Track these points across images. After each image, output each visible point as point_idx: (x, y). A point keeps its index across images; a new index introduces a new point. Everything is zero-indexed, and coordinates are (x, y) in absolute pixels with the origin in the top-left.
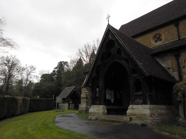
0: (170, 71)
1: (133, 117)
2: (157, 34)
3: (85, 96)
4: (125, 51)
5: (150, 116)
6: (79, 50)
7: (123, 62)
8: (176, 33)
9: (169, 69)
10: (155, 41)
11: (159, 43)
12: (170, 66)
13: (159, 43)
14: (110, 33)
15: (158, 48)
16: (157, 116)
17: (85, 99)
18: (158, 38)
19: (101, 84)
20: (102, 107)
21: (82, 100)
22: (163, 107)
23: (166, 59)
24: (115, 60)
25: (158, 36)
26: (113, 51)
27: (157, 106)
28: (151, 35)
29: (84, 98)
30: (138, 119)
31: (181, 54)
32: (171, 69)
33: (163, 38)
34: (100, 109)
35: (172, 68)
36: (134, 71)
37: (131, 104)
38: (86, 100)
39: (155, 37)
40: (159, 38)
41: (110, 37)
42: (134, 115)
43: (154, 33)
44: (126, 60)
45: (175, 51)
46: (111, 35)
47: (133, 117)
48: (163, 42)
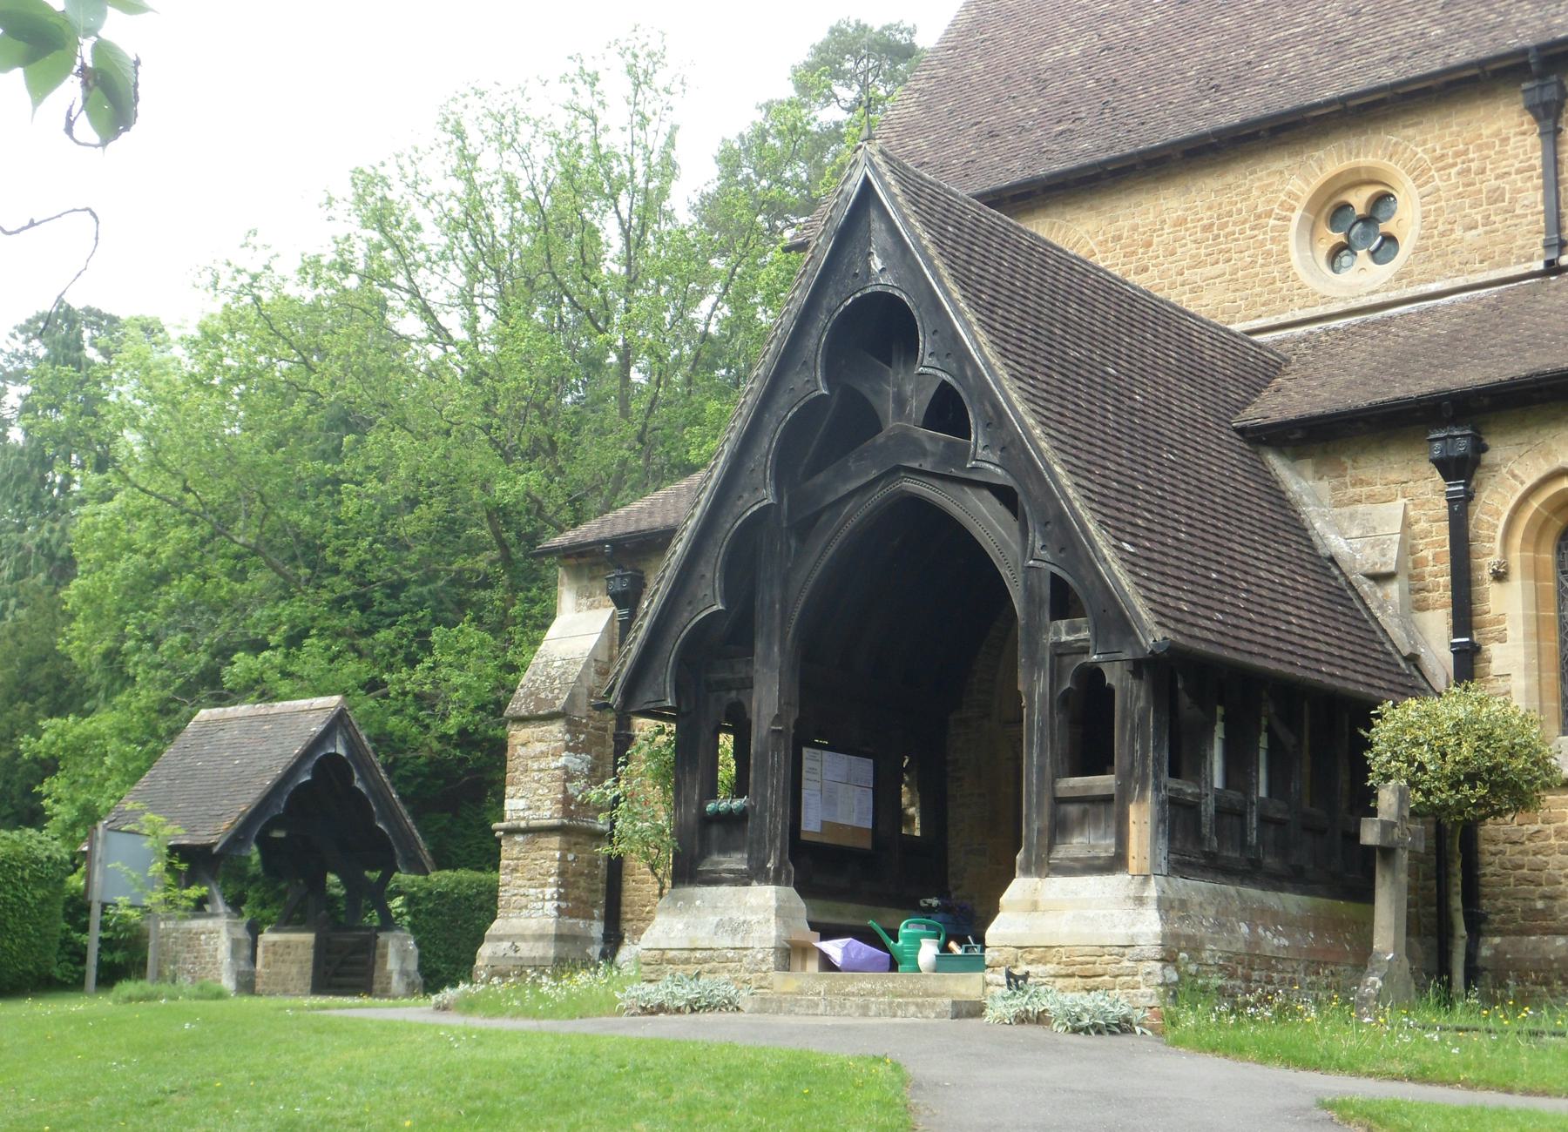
0: (1387, 602)
1: (1031, 969)
2: (1356, 170)
3: (548, 814)
4: (997, 420)
5: (1161, 960)
6: (365, 182)
7: (984, 518)
8: (1533, 197)
9: (1380, 578)
10: (1324, 248)
11: (1364, 279)
12: (1393, 552)
13: (1364, 279)
14: (877, 225)
15: (1347, 333)
16: (1222, 968)
17: (555, 840)
18: (1355, 223)
19: (767, 700)
20: (773, 903)
21: (510, 851)
22: (1290, 902)
23: (1365, 490)
24: (912, 485)
25: (1359, 200)
26: (905, 393)
27: (1231, 890)
28: (1291, 181)
29: (535, 832)
30: (1073, 981)
31: (1487, 458)
32: (1393, 590)
33: (1405, 221)
34: (753, 918)
35: (1411, 577)
36: (1063, 602)
37: (1027, 871)
38: (563, 859)
39: (1332, 209)
40: (1369, 220)
41: (877, 264)
42: (1044, 953)
43: (1328, 161)
44: (1006, 496)
45: (1451, 426)
46: (885, 256)
47: (1031, 969)
48: (1400, 277)
